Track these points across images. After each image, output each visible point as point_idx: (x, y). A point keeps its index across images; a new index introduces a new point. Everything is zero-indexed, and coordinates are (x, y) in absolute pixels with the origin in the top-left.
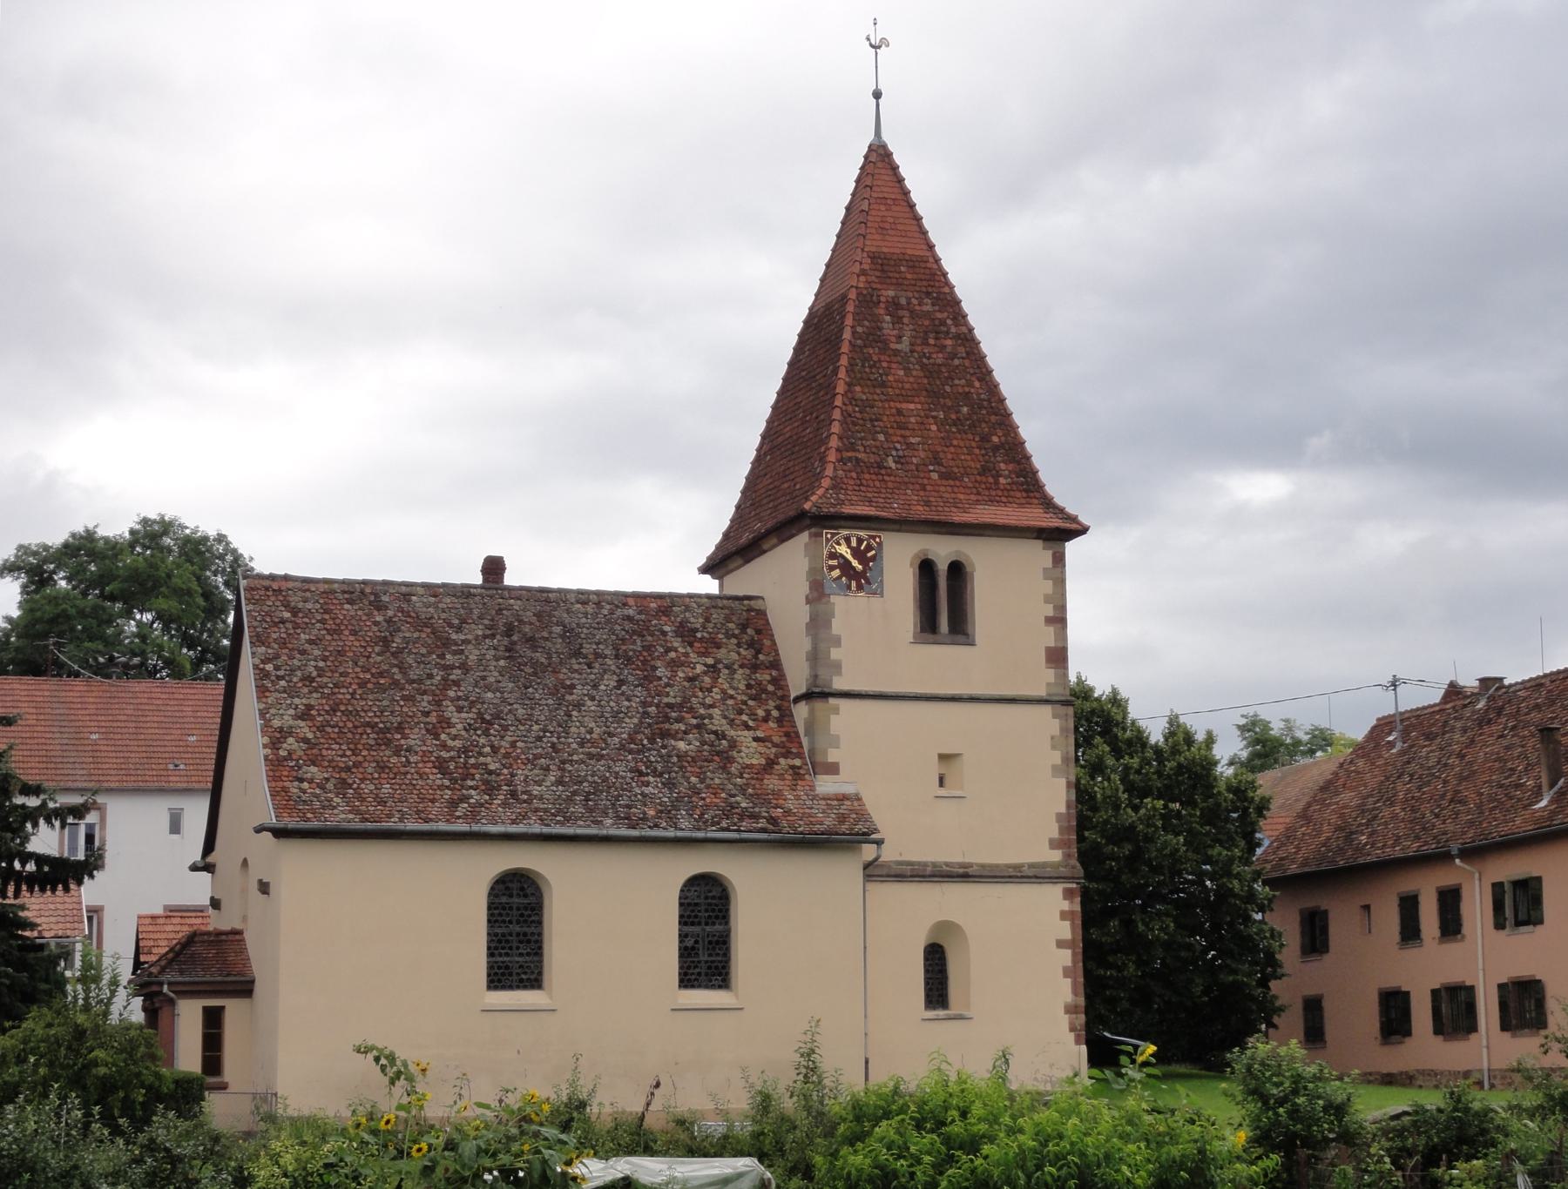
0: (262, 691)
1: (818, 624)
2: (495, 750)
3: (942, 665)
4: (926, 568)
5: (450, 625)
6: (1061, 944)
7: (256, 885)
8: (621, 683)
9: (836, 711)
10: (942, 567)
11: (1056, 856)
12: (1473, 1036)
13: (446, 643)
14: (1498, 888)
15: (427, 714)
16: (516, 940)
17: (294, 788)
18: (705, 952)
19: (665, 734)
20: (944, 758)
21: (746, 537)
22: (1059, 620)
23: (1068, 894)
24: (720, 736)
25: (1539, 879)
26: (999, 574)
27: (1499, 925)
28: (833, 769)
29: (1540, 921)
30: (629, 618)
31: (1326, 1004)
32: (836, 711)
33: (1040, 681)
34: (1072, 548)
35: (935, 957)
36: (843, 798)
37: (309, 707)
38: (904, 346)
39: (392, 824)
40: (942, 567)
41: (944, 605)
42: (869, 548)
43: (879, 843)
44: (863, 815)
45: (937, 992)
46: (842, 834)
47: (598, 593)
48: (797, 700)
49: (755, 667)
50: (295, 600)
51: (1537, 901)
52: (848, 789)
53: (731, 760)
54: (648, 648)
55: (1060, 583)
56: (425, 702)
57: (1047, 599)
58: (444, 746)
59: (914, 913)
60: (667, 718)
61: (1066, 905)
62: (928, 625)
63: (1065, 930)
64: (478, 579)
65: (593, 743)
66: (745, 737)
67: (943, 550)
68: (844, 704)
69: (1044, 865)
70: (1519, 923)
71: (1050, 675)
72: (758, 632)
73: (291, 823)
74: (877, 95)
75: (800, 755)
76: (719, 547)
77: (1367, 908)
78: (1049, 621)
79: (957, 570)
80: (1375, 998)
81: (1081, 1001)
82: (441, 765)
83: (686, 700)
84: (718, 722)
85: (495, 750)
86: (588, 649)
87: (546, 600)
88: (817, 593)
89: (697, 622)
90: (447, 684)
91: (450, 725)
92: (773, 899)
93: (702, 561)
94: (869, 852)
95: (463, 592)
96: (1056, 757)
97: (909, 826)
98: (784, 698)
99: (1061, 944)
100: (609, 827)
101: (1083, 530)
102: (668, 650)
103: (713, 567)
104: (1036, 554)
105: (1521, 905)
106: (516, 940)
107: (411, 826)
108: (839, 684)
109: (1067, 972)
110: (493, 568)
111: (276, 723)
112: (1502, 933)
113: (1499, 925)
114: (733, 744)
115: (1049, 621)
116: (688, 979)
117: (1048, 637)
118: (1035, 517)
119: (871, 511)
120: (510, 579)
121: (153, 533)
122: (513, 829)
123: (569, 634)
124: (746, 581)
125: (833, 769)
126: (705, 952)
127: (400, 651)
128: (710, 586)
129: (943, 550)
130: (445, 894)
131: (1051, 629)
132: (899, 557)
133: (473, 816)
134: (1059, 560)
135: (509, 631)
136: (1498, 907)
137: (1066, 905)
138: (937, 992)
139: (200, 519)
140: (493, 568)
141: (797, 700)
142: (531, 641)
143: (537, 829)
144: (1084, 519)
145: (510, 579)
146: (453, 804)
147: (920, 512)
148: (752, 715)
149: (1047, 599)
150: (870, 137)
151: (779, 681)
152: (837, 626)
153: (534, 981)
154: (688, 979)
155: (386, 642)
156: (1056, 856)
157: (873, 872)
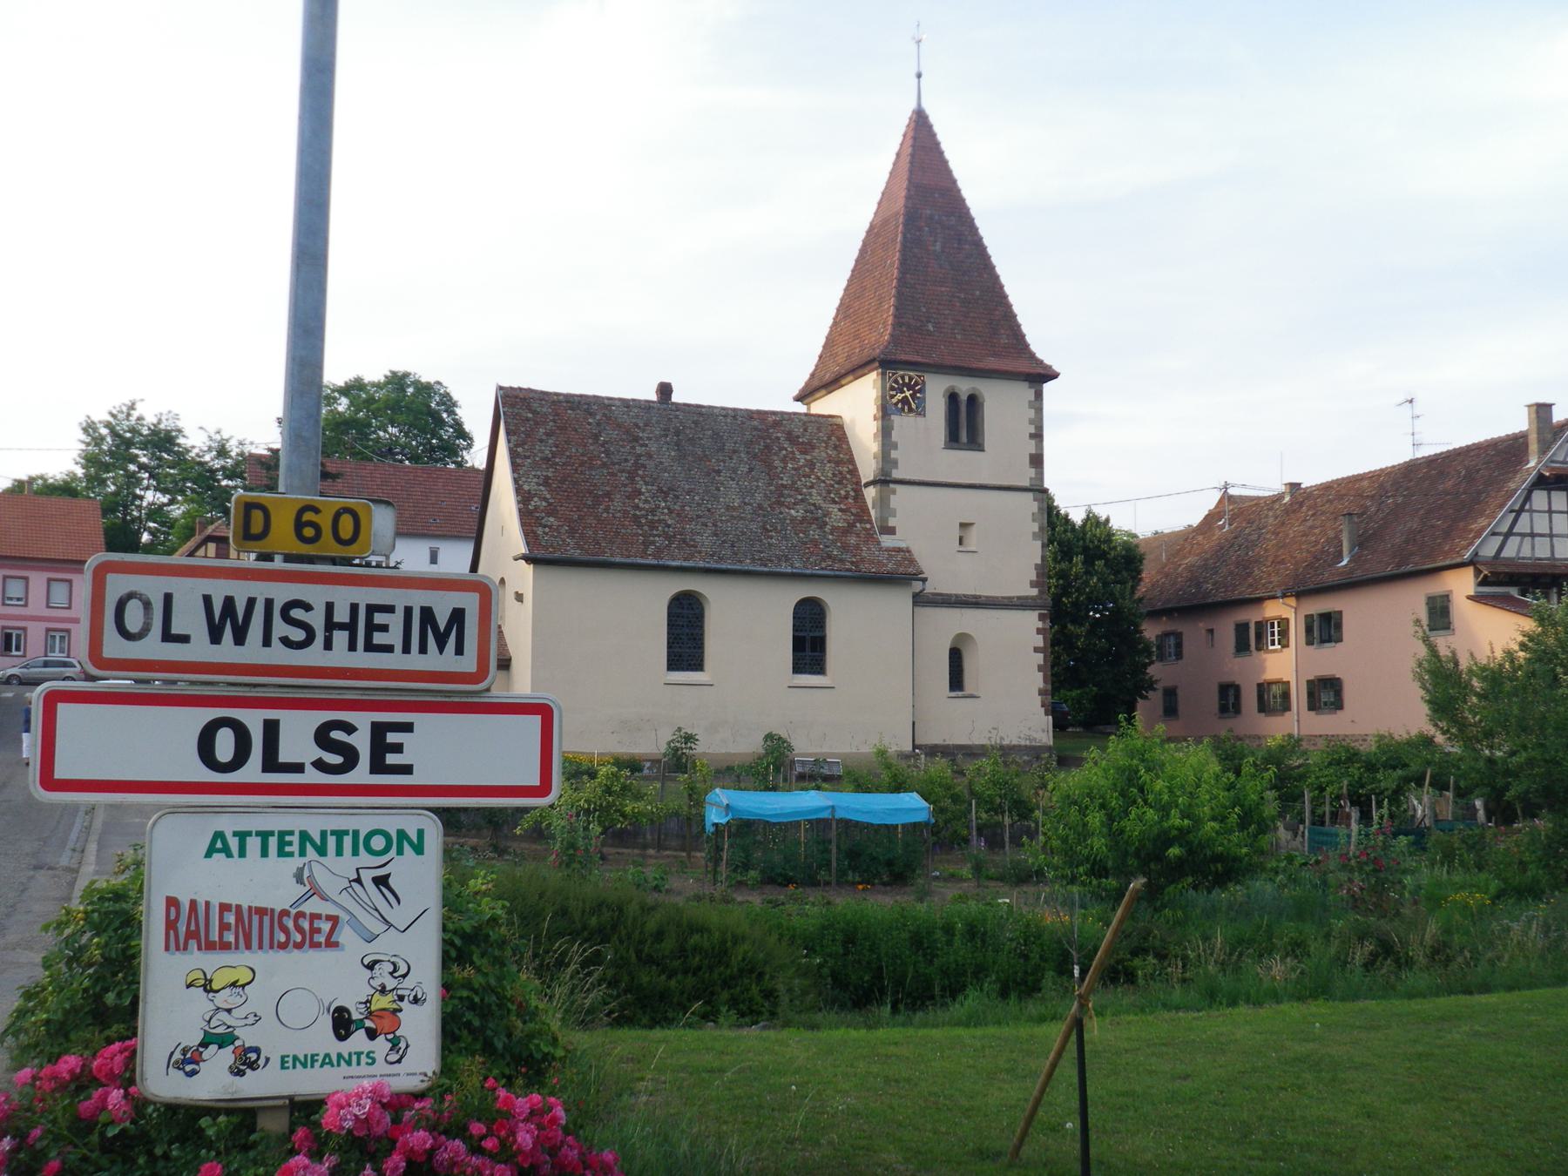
0: (515, 467)
1: (886, 432)
2: (671, 511)
3: (962, 464)
4: (953, 398)
5: (636, 425)
6: (1036, 650)
7: (513, 596)
8: (751, 470)
9: (894, 492)
10: (964, 397)
11: (1034, 592)
12: (1287, 714)
13: (636, 439)
14: (1309, 618)
15: (625, 486)
16: (686, 642)
17: (540, 531)
18: (809, 648)
19: (781, 504)
20: (964, 526)
21: (828, 377)
22: (1038, 436)
23: (1041, 618)
24: (818, 507)
25: (1340, 613)
26: (1001, 404)
27: (1309, 642)
28: (891, 531)
29: (1340, 640)
30: (756, 429)
31: (1180, 693)
32: (894, 492)
33: (1025, 477)
34: (1048, 387)
35: (956, 657)
36: (899, 550)
37: (547, 478)
38: (938, 247)
39: (606, 557)
40: (964, 397)
41: (964, 425)
42: (916, 384)
43: (924, 580)
44: (912, 561)
45: (956, 681)
46: (898, 574)
47: (734, 410)
48: (867, 485)
49: (838, 463)
50: (535, 405)
51: (1339, 626)
52: (903, 545)
53: (826, 524)
54: (767, 447)
55: (1039, 410)
56: (623, 477)
57: (1031, 422)
58: (637, 507)
59: (947, 625)
60: (781, 495)
61: (1040, 625)
62: (953, 440)
63: (1039, 641)
64: (654, 397)
65: (734, 509)
66: (834, 509)
67: (964, 386)
68: (899, 488)
69: (1026, 598)
70: (1322, 641)
71: (1032, 472)
72: (839, 439)
73: (540, 554)
74: (919, 76)
75: (870, 521)
76: (807, 384)
77: (1211, 631)
78: (1032, 436)
79: (973, 400)
80: (1215, 689)
81: (1049, 687)
82: (636, 519)
83: (794, 483)
84: (816, 498)
85: (671, 511)
86: (729, 446)
87: (700, 415)
88: (886, 412)
89: (798, 431)
90: (637, 466)
91: (640, 493)
92: (854, 617)
93: (796, 392)
94: (917, 586)
95: (646, 406)
96: (1035, 527)
97: (945, 571)
98: (858, 483)
99: (1036, 650)
100: (748, 565)
101: (1054, 376)
102: (782, 449)
103: (800, 398)
104: (1024, 392)
105: (1326, 629)
106: (686, 642)
107: (618, 559)
108: (896, 474)
109: (1040, 668)
110: (665, 390)
111: (526, 487)
112: (1311, 648)
113: (1309, 642)
114: (827, 514)
115: (1032, 436)
116: (797, 669)
117: (1031, 447)
118: (1023, 366)
119: (919, 359)
120: (677, 397)
121: (398, 381)
122: (685, 564)
123: (716, 436)
124: (824, 406)
125: (891, 531)
126: (809, 648)
127: (605, 442)
128: (800, 408)
129: (964, 386)
130: (644, 603)
131: (1033, 442)
132: (936, 390)
133: (658, 553)
134: (1039, 395)
135: (677, 433)
136: (1309, 630)
137: (1040, 625)
138: (956, 681)
139: (426, 374)
140: (665, 390)
141: (867, 485)
142: (691, 440)
143: (701, 564)
144: (1056, 368)
145: (677, 397)
146: (646, 544)
147: (949, 360)
148: (837, 493)
149: (1031, 422)
150: (913, 105)
151: (854, 472)
152: (895, 436)
153: (697, 664)
154: (797, 669)
155: (596, 437)
156: (1034, 592)
157: (920, 600)
